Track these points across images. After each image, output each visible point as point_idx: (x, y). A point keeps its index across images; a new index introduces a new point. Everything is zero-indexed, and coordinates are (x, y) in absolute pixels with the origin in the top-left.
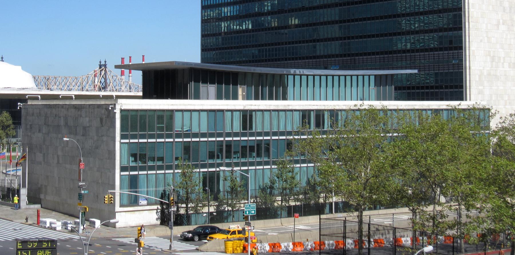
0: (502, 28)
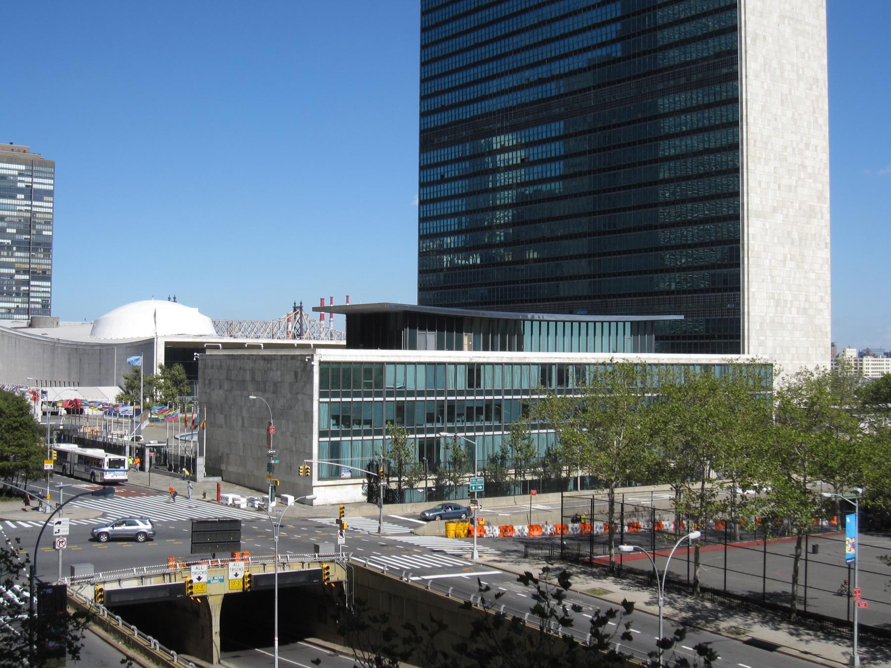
0: (790, 264)
